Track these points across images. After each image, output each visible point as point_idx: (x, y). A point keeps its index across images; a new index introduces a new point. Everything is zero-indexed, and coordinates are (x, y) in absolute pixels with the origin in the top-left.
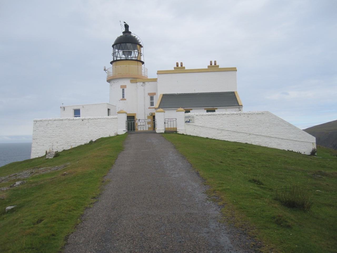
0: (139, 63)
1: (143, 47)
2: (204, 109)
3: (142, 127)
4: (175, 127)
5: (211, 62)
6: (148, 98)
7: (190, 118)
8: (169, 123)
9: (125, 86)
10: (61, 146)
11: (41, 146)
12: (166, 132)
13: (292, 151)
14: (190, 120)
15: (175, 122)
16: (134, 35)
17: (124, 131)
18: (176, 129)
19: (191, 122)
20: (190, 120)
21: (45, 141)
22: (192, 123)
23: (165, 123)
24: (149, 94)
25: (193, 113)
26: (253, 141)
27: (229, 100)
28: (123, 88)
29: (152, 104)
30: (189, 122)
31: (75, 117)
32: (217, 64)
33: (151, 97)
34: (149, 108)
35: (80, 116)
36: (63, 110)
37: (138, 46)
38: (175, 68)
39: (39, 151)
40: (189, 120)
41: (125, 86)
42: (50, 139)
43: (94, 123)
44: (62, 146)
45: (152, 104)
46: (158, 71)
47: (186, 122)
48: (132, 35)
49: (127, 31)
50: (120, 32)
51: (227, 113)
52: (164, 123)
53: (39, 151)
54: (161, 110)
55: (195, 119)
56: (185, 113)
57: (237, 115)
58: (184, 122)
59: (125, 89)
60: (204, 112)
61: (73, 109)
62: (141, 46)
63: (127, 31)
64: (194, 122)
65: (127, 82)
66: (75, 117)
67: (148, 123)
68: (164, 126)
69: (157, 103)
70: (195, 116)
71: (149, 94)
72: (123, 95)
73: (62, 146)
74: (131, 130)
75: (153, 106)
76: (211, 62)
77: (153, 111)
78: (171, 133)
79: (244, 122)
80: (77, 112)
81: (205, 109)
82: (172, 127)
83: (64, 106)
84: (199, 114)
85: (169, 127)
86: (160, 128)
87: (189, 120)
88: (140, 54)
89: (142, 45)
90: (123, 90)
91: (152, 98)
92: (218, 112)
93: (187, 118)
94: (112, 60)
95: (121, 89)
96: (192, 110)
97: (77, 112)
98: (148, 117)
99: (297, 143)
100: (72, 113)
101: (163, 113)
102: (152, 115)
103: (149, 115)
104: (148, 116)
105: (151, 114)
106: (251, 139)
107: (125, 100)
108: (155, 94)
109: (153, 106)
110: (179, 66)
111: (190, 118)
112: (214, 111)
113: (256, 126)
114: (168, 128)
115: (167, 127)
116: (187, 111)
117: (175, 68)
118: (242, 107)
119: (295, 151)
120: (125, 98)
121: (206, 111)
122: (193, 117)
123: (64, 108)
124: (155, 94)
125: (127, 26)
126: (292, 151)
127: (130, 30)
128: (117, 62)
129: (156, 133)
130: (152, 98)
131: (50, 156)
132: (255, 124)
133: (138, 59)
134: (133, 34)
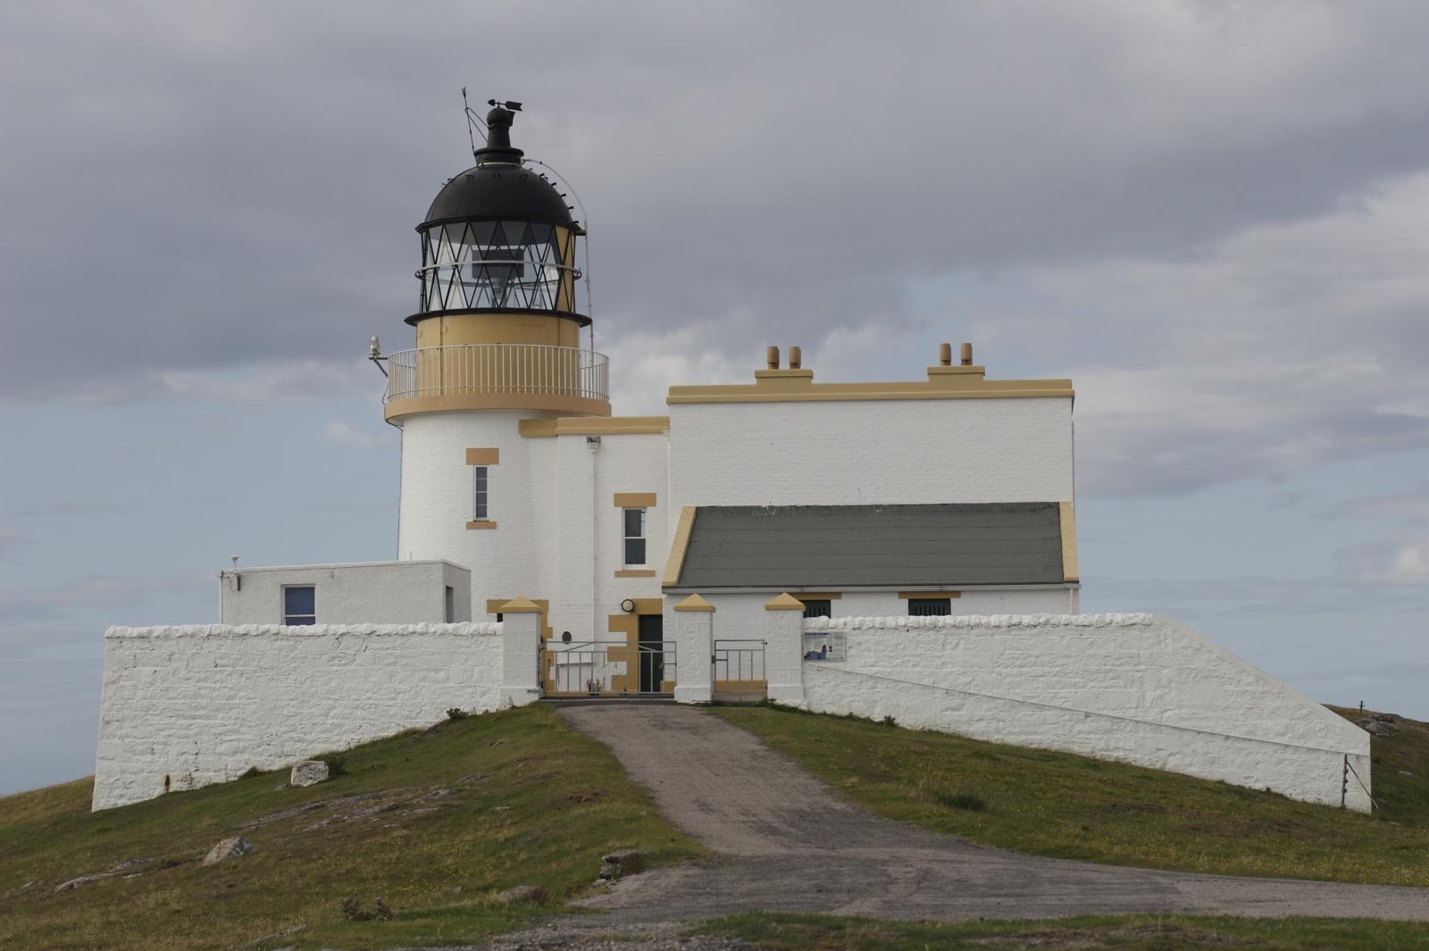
0: (567, 324)
1: (584, 234)
2: (897, 597)
3: (574, 672)
4: (758, 677)
5: (947, 349)
6: (616, 520)
7: (825, 641)
8: (733, 657)
9: (492, 455)
10: (239, 757)
11: (142, 753)
12: (715, 705)
13: (1268, 789)
14: (824, 647)
15: (758, 656)
16: (537, 170)
17: (529, 691)
18: (763, 685)
19: (803, 667)
20: (824, 647)
21: (163, 733)
22: (835, 660)
23: (714, 660)
24: (619, 499)
25: (846, 616)
26: (1102, 745)
27: (1013, 546)
28: (482, 465)
29: (635, 552)
30: (820, 657)
31: (292, 628)
32: (976, 362)
33: (626, 511)
34: (618, 574)
35: (311, 621)
36: (235, 586)
37: (562, 234)
38: (760, 376)
39: (133, 777)
40: (820, 651)
41: (492, 455)
42: (187, 722)
43: (391, 654)
44: (245, 756)
45: (635, 552)
46: (673, 390)
47: (808, 657)
48: (526, 166)
49: (500, 150)
50: (458, 151)
51: (984, 620)
52: (709, 660)
53: (133, 777)
54: (695, 600)
55: (848, 645)
56: (805, 615)
57: (1035, 631)
58: (799, 658)
59: (492, 470)
60: (895, 613)
61: (282, 586)
62: (574, 230)
63: (500, 150)
64: (842, 660)
65: (497, 434)
66: (289, 622)
67: (614, 654)
68: (709, 672)
69: (666, 538)
70: (848, 629)
71: (619, 499)
72: (481, 499)
73: (245, 756)
74: (654, 691)
75: (642, 561)
76: (947, 349)
77: (647, 590)
78: (740, 706)
79: (1060, 661)
80: (299, 603)
81: (902, 594)
82: (746, 677)
83: (240, 568)
84: (870, 623)
85: (734, 677)
86: (690, 680)
87: (820, 651)
88: (568, 274)
89: (581, 225)
90: (481, 473)
91: (633, 521)
92: (965, 611)
93: (813, 641)
94: (415, 310)
95: (471, 470)
96: (840, 598)
97: (299, 603)
98: (615, 624)
99: (1288, 755)
100: (277, 602)
101: (708, 615)
102: (632, 611)
103: (619, 612)
104: (611, 618)
105: (628, 606)
106: (1092, 736)
107: (493, 526)
108: (651, 499)
109: (642, 561)
110: (781, 367)
111: (825, 641)
112: (942, 607)
113: (1114, 678)
114: (1343, 808)
115: (721, 677)
116: (817, 607)
117: (760, 376)
118: (1076, 590)
119: (1279, 791)
120: (492, 515)
121: (906, 602)
122: (839, 636)
123: (239, 579)
124: (651, 499)
125: (501, 120)
126: (1268, 789)
127: (515, 143)
128: (447, 320)
129: (676, 703)
130: (633, 521)
131: (310, 776)
132: (1111, 670)
133: (563, 307)
134: (531, 164)
